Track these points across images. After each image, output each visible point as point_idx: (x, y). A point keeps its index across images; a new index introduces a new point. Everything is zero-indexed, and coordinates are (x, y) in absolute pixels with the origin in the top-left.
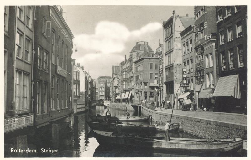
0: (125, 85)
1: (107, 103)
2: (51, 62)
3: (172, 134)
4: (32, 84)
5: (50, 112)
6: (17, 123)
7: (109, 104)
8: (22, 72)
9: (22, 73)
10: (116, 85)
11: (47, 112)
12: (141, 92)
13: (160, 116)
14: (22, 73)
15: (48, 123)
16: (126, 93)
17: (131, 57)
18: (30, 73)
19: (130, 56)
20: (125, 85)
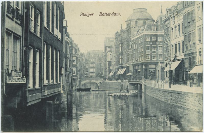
0: (120, 59)
1: (100, 81)
2: (44, 25)
3: (73, 104)
4: (22, 50)
5: (42, 86)
6: (156, 129)
7: (102, 82)
8: (12, 34)
9: (13, 35)
10: (110, 60)
11: (39, 86)
12: (156, 125)
13: (200, 26)
14: (13, 35)
15: (40, 100)
16: (123, 69)
17: (128, 26)
18: (20, 36)
19: (127, 25)
20: (120, 59)
